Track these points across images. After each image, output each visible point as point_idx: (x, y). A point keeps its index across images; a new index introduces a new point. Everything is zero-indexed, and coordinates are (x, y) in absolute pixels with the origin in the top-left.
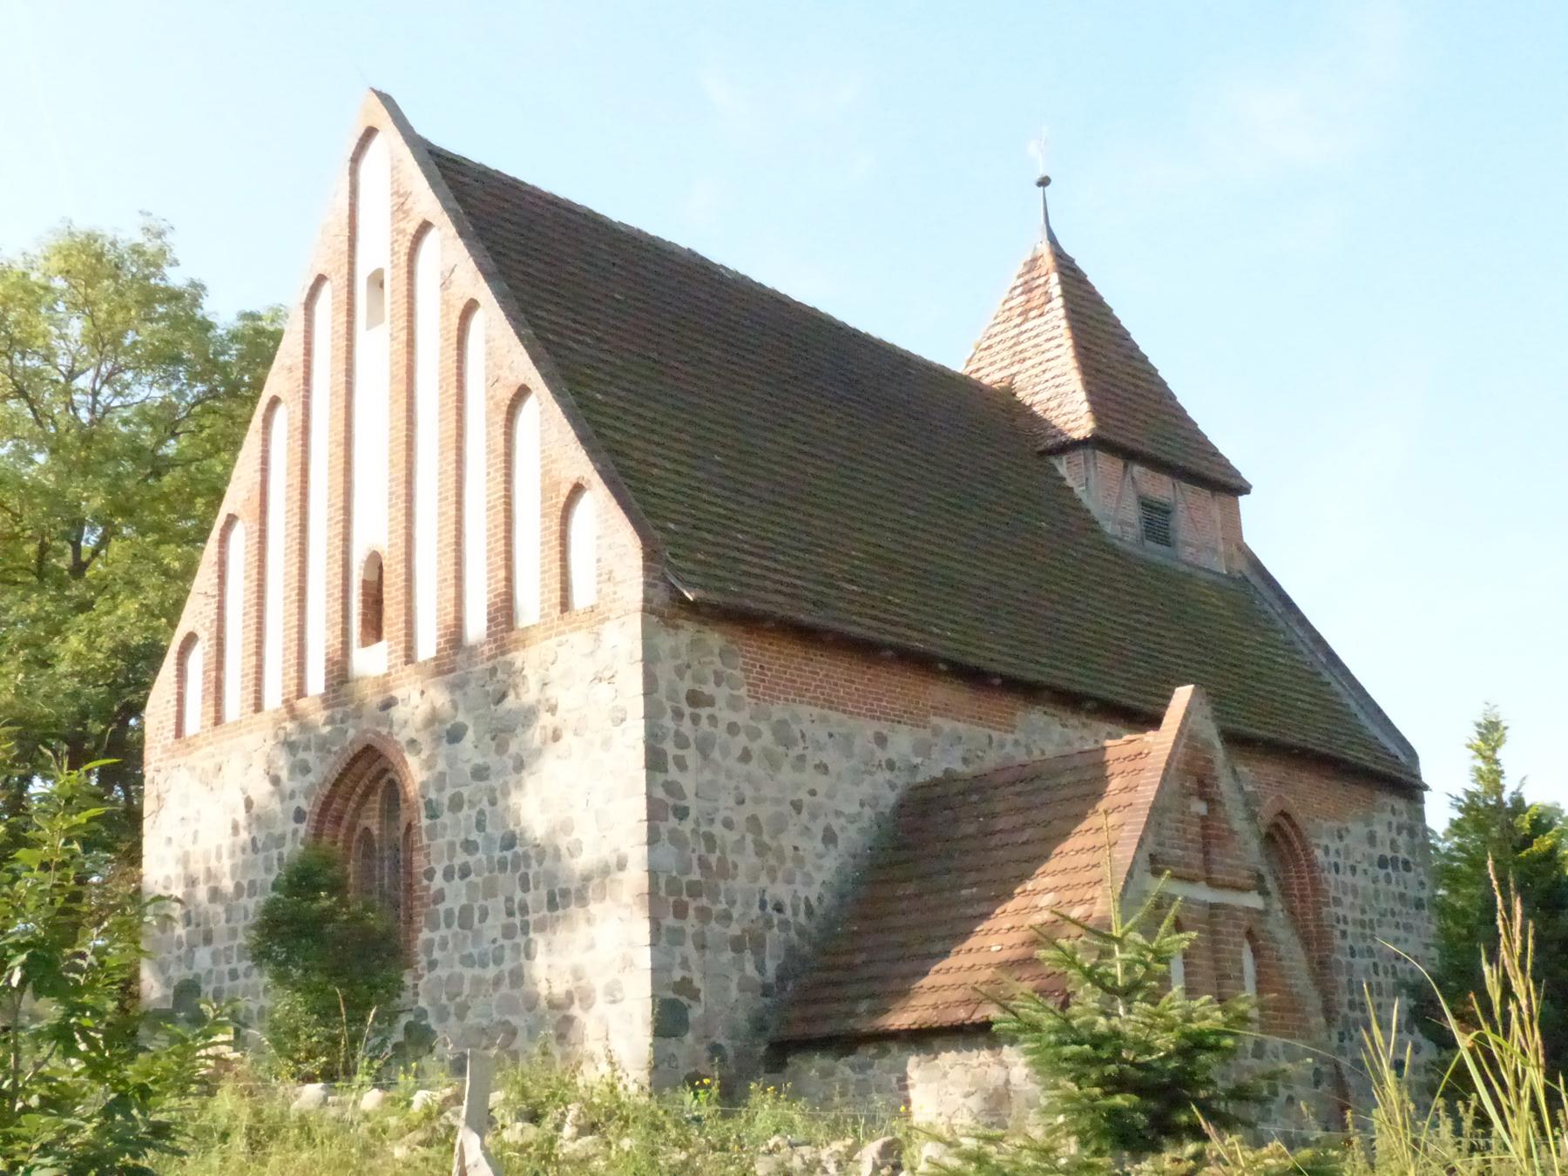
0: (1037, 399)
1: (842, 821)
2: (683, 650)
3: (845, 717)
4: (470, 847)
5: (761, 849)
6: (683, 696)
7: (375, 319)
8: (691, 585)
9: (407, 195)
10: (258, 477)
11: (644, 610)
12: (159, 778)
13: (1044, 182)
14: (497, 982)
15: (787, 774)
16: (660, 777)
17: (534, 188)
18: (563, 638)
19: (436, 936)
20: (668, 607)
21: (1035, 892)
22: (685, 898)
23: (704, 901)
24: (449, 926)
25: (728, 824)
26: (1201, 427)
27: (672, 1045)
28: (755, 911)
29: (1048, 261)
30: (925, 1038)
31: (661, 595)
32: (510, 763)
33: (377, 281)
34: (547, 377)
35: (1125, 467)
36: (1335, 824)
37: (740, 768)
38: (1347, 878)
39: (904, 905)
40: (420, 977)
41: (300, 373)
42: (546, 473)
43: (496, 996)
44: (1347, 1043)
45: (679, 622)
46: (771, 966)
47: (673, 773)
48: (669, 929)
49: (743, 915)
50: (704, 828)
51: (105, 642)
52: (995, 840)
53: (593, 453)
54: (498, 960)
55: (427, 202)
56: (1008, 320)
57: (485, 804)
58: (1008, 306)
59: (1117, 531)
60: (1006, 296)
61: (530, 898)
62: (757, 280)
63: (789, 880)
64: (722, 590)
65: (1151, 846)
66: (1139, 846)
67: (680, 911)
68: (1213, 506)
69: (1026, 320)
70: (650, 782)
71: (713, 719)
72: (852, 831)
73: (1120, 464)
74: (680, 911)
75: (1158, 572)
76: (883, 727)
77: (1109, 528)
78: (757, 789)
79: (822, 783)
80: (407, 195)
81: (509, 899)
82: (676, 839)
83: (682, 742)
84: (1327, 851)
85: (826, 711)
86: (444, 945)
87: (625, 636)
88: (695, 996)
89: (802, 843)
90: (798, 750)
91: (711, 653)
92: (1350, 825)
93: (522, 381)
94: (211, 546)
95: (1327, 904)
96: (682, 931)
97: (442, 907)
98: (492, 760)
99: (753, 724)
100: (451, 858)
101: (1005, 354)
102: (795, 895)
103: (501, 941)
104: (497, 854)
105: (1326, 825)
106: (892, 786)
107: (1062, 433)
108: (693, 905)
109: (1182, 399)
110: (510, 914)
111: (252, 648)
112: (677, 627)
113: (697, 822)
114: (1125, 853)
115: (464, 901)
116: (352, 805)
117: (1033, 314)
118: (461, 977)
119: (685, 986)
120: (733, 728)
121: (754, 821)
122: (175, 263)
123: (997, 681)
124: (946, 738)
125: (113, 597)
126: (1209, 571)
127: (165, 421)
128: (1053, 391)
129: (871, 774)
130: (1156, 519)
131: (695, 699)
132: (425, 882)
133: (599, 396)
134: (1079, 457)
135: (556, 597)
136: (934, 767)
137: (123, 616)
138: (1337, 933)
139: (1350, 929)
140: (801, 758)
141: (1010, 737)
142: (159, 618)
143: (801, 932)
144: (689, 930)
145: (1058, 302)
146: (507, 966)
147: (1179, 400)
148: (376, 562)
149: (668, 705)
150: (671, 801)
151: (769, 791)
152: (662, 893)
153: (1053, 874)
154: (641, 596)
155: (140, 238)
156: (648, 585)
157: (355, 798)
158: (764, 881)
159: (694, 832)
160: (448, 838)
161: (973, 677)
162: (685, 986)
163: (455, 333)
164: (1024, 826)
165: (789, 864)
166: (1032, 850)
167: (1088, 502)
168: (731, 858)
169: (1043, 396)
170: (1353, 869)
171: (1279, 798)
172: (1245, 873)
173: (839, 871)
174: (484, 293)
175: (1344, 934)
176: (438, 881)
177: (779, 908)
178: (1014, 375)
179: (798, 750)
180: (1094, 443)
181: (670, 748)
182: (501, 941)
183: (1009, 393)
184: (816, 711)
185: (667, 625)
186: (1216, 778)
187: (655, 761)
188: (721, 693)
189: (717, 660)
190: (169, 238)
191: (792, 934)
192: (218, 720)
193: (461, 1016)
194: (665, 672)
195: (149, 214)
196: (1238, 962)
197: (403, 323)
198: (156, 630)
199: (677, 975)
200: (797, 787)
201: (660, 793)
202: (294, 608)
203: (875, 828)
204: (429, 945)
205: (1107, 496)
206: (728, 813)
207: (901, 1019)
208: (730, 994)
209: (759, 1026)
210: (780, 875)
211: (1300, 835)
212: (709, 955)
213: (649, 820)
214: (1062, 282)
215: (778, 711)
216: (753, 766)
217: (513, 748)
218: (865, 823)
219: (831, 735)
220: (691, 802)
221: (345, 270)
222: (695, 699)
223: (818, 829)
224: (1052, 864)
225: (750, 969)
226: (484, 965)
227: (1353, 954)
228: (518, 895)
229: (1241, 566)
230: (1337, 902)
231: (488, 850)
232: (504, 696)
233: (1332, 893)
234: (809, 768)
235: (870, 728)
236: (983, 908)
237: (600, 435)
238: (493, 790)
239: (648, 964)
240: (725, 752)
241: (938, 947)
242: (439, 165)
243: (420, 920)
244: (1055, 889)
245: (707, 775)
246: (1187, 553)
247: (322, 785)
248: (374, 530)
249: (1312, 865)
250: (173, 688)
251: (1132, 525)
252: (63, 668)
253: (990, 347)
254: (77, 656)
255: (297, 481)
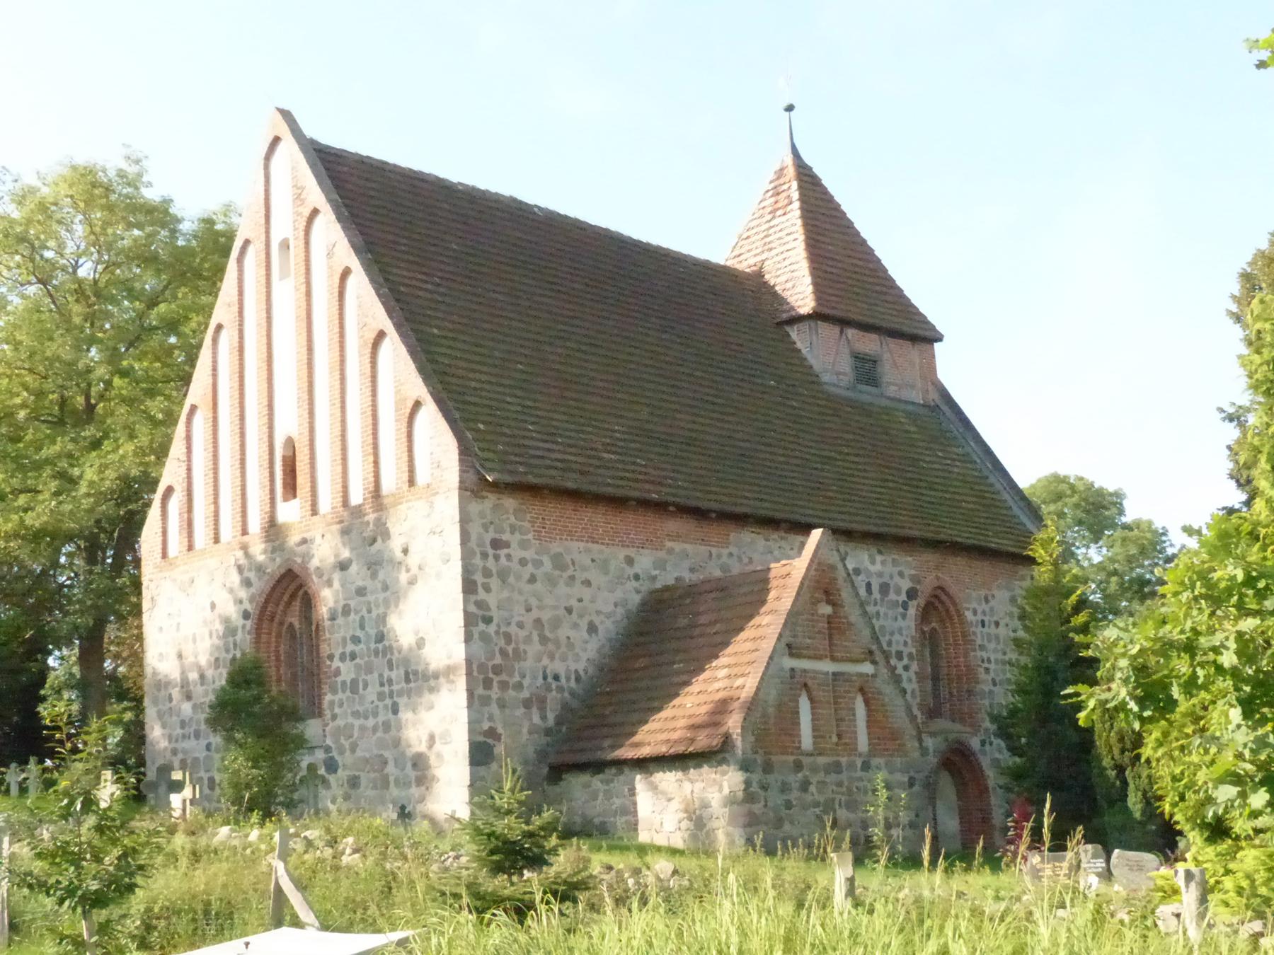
0: (778, 280)
1: (602, 617)
2: (488, 512)
3: (603, 547)
4: (356, 640)
5: (544, 640)
6: (488, 543)
7: (284, 275)
8: (490, 470)
9: (303, 188)
10: (210, 381)
11: (460, 488)
12: (152, 586)
13: (790, 108)
14: (375, 729)
15: (562, 589)
16: (473, 598)
17: (395, 166)
18: (410, 504)
19: (336, 698)
20: (475, 486)
21: (717, 668)
22: (491, 675)
23: (504, 677)
24: (344, 691)
25: (520, 625)
26: (906, 293)
27: (482, 771)
28: (540, 680)
29: (791, 172)
30: (646, 764)
31: (472, 477)
32: (379, 586)
33: (285, 245)
34: (398, 327)
35: (842, 332)
36: (983, 593)
37: (529, 587)
38: (993, 630)
39: (638, 675)
40: (327, 725)
41: (235, 309)
42: (398, 392)
43: (374, 738)
44: (987, 747)
45: (484, 494)
46: (551, 717)
47: (482, 595)
48: (480, 696)
49: (530, 685)
50: (503, 629)
51: (111, 474)
52: (697, 631)
53: (427, 379)
54: (375, 714)
55: (316, 195)
56: (762, 216)
57: (364, 612)
58: (763, 205)
59: (834, 379)
60: (761, 198)
61: (394, 675)
62: (562, 212)
63: (564, 659)
64: (511, 472)
65: (785, 640)
66: (778, 639)
67: (487, 684)
68: (914, 352)
69: (774, 218)
70: (465, 602)
71: (509, 557)
72: (609, 624)
73: (837, 330)
74: (487, 684)
75: (865, 410)
76: (631, 552)
77: (826, 378)
78: (540, 600)
79: (586, 593)
80: (303, 188)
81: (381, 676)
82: (485, 637)
83: (487, 573)
84: (975, 613)
85: (590, 545)
86: (341, 705)
87: (448, 505)
88: (497, 737)
89: (572, 634)
90: (570, 572)
91: (507, 513)
92: (995, 592)
93: (381, 327)
94: (180, 429)
95: (974, 650)
96: (489, 697)
97: (339, 679)
98: (368, 583)
99: (536, 557)
100: (344, 647)
101: (758, 244)
102: (568, 670)
103: (377, 703)
104: (373, 646)
105: (974, 594)
106: (638, 592)
107: (792, 308)
108: (496, 679)
109: (892, 272)
110: (382, 685)
111: (211, 499)
112: (483, 498)
113: (498, 626)
114: (768, 646)
115: (353, 676)
116: (281, 607)
117: (779, 213)
118: (353, 726)
119: (492, 733)
120: (523, 562)
121: (538, 622)
122: (149, 185)
123: (714, 515)
124: (678, 556)
125: (116, 440)
126: (906, 402)
127: (149, 292)
128: (789, 276)
129: (622, 584)
130: (867, 369)
131: (496, 544)
132: (328, 663)
133: (435, 331)
134: (805, 326)
135: (405, 477)
136: (667, 579)
137: (123, 455)
138: (982, 670)
139: (992, 666)
140: (572, 578)
141: (725, 552)
142: (149, 455)
143: (572, 694)
144: (494, 697)
145: (797, 205)
146: (381, 719)
147: (890, 272)
148: (290, 443)
149: (478, 550)
150: (480, 613)
151: (549, 601)
152: (475, 673)
153: (729, 656)
154: (457, 479)
155: (124, 165)
156: (462, 471)
157: (283, 603)
158: (545, 661)
159: (497, 633)
160: (342, 634)
161: (698, 514)
162: (492, 733)
163: (337, 290)
164: (716, 622)
165: (563, 649)
166: (718, 639)
167: (812, 361)
168: (522, 647)
169: (783, 278)
170: (997, 624)
171: (938, 578)
172: (859, 650)
173: (599, 651)
174: (354, 263)
175: (987, 670)
176: (337, 663)
177: (556, 678)
178: (763, 261)
179: (570, 572)
180: (816, 316)
181: (479, 578)
182: (377, 703)
183: (759, 275)
184: (582, 545)
185: (476, 497)
186: (838, 590)
187: (469, 587)
188: (515, 539)
189: (512, 519)
190: (144, 163)
191: (566, 694)
192: (190, 548)
193: (353, 750)
194: (475, 529)
195: (129, 146)
196: (852, 711)
197: (302, 279)
198: (147, 464)
199: (486, 726)
200: (569, 596)
201: (473, 608)
202: (238, 473)
203: (625, 620)
204: (332, 703)
205: (827, 356)
206: (521, 619)
207: (626, 753)
208: (522, 733)
209: (542, 754)
210: (557, 656)
211: (955, 604)
212: (507, 711)
213: (465, 626)
214: (800, 188)
215: (556, 547)
216: (538, 586)
217: (381, 575)
218: (619, 617)
219: (593, 561)
220: (494, 613)
221: (263, 237)
222: (496, 544)
223: (584, 624)
224: (730, 650)
225: (536, 719)
226: (366, 718)
227: (995, 684)
228: (386, 673)
229: (933, 396)
230: (982, 647)
231: (367, 643)
232: (374, 540)
233: (979, 642)
234: (578, 582)
235: (622, 553)
236: (685, 678)
237: (432, 361)
238: (369, 603)
239: (466, 720)
240: (518, 577)
241: (656, 704)
242: (322, 160)
243: (326, 688)
244: (728, 666)
245: (505, 594)
246: (891, 391)
247: (260, 595)
248: (289, 424)
249: (962, 621)
250: (160, 524)
251: (845, 374)
252: (83, 488)
253: (748, 237)
254: (91, 484)
255: (236, 385)
